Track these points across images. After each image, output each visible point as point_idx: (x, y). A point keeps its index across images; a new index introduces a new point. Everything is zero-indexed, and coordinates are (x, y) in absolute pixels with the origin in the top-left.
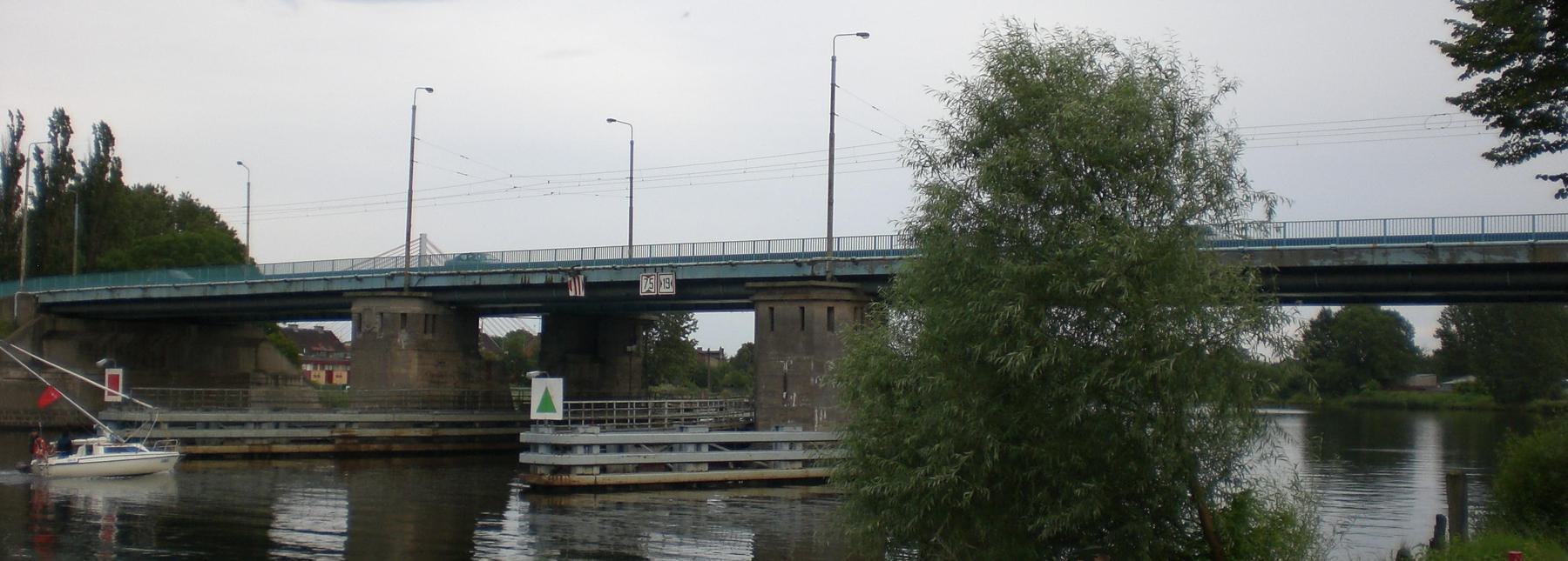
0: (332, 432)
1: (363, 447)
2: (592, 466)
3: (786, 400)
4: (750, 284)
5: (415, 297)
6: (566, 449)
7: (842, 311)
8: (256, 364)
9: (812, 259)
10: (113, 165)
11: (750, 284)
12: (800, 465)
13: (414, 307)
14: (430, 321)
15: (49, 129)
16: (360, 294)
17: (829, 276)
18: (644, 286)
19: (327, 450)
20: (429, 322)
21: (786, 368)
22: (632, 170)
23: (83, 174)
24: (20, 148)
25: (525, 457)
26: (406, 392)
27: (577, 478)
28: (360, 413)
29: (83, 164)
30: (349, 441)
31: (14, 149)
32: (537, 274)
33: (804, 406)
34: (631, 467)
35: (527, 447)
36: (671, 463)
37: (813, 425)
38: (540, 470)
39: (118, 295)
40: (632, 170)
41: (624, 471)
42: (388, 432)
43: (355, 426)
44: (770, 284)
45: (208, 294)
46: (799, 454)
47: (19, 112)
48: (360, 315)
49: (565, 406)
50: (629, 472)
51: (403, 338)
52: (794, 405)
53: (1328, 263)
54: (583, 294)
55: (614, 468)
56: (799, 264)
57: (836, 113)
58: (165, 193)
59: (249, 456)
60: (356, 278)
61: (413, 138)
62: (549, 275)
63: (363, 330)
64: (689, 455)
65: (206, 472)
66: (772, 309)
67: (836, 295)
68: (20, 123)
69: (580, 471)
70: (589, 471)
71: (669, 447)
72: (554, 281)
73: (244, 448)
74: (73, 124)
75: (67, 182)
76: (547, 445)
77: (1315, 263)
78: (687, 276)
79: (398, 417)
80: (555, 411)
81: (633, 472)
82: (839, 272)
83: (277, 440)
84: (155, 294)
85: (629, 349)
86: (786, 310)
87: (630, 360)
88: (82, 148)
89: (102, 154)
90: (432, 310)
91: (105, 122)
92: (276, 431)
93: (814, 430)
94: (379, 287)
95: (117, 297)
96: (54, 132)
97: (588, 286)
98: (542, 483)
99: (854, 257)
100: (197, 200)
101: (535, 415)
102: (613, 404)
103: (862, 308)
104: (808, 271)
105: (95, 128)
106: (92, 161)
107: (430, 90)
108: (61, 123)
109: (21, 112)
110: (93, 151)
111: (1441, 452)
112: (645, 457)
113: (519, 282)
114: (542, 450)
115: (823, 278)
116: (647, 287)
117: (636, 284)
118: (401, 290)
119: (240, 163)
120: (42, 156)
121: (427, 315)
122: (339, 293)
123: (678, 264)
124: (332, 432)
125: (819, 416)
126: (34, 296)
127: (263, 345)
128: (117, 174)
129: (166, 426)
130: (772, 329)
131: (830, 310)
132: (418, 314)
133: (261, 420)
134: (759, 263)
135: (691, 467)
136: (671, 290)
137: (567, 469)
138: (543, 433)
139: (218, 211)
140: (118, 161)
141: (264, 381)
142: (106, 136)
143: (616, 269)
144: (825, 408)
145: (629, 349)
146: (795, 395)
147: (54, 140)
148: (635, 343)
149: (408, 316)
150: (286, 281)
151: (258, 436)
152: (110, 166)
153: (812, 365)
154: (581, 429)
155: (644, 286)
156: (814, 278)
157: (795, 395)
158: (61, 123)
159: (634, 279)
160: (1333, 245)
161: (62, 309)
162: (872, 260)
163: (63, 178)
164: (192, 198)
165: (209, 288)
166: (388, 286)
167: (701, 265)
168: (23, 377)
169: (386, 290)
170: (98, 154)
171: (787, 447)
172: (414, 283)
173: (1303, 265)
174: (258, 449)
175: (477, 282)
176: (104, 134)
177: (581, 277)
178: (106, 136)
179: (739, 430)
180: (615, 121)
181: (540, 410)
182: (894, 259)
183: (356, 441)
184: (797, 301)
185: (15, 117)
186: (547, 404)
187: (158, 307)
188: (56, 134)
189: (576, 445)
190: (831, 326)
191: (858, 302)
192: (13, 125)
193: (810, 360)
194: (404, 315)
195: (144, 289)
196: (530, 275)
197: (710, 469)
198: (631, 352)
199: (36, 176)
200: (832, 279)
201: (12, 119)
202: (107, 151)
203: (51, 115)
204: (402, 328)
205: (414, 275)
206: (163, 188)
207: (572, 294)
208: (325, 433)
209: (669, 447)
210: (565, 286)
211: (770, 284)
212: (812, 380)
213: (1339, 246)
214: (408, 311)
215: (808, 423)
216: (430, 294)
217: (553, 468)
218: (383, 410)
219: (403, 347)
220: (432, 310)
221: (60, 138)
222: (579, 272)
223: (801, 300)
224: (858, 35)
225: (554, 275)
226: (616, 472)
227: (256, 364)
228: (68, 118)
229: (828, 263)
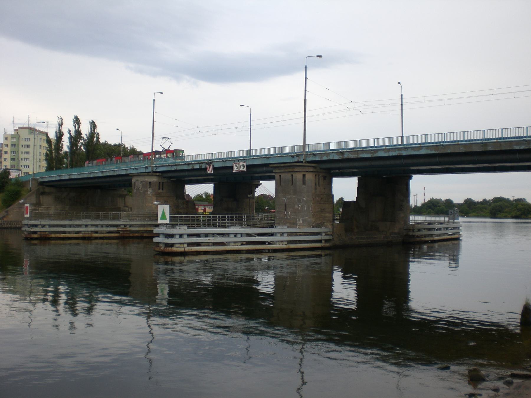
0: (118, 229)
1: (131, 235)
2: (183, 243)
3: (286, 215)
4: (271, 166)
5: (154, 175)
6: (172, 236)
7: (310, 177)
8: (125, 204)
9: (298, 155)
10: (96, 135)
11: (271, 166)
12: (286, 243)
13: (154, 179)
14: (161, 185)
15: (73, 123)
16: (134, 174)
17: (304, 161)
18: (234, 168)
19: (116, 236)
20: (161, 185)
21: (286, 201)
22: (250, 126)
23: (86, 138)
24: (62, 129)
25: (156, 240)
26: (151, 213)
27: (175, 249)
28: (130, 221)
29: (86, 135)
30: (125, 232)
31: (60, 130)
32: (196, 165)
33: (293, 217)
34: (245, 243)
35: (158, 235)
36: (226, 242)
37: (297, 226)
38: (161, 245)
39: (62, 178)
40: (250, 126)
41: (208, 245)
42: (142, 229)
43: (128, 226)
44: (279, 165)
45: (89, 177)
46: (286, 238)
47: (61, 117)
48: (135, 182)
49: (170, 217)
50: (210, 246)
51: (150, 192)
52: (289, 217)
53: (523, 147)
54: (212, 172)
55: (203, 244)
56: (293, 157)
57: (307, 90)
58: (125, 146)
59: (83, 238)
60: (135, 168)
61: (154, 112)
62: (201, 165)
63: (136, 189)
64: (231, 239)
65: (102, 244)
66: (280, 176)
67: (306, 169)
68: (62, 121)
69: (177, 245)
70: (182, 245)
71: (223, 235)
72: (202, 167)
73: (80, 235)
74: (81, 121)
75: (80, 141)
76: (163, 234)
77: (517, 148)
78: (251, 163)
79: (146, 223)
80: (166, 219)
81: (212, 246)
82: (308, 159)
83: (102, 232)
84: (73, 177)
85: (249, 196)
86: (286, 176)
87: (250, 200)
88: (85, 130)
89: (93, 131)
90: (161, 180)
91: (93, 120)
92: (85, 228)
93: (297, 228)
94: (143, 172)
95: (61, 179)
96: (75, 124)
97: (215, 169)
98: (161, 251)
99: (314, 154)
100: (136, 148)
101: (160, 221)
102: (237, 216)
103: (319, 175)
104: (296, 159)
105: (90, 122)
106: (90, 134)
107: (162, 93)
108: (77, 121)
109: (62, 117)
110: (90, 130)
111: (67, 240)
112: (209, 239)
113: (190, 168)
114: (161, 236)
115: (302, 162)
116: (235, 169)
117: (231, 167)
118: (150, 172)
119: (117, 129)
120: (71, 132)
121: (159, 183)
122: (127, 175)
123: (247, 158)
124: (118, 229)
125: (299, 221)
126: (37, 179)
127: (127, 197)
128: (98, 138)
129: (48, 227)
130: (281, 185)
131: (304, 176)
132: (156, 182)
133: (87, 224)
134: (277, 157)
135: (232, 244)
136: (244, 169)
137: (172, 245)
138: (162, 229)
139: (436, 196)
140: (98, 133)
141: (128, 210)
142: (93, 125)
143: (224, 161)
144: (302, 218)
145: (249, 196)
146: (289, 212)
147: (75, 127)
148: (252, 194)
149: (152, 182)
150: (112, 171)
151: (87, 230)
152: (95, 136)
153: (296, 200)
154: (178, 227)
155: (234, 168)
156: (298, 162)
157: (289, 212)
158: (77, 121)
159: (231, 165)
160: (524, 139)
161: (47, 184)
162: (322, 153)
163: (78, 140)
164: (134, 148)
165: (89, 174)
166: (146, 171)
167: (255, 158)
168: (32, 209)
169: (146, 172)
170: (91, 132)
171: (232, 236)
172: (155, 169)
173: (510, 149)
174: (86, 236)
175: (176, 169)
176: (93, 124)
177: (212, 165)
178: (93, 125)
179: (270, 228)
180: (243, 106)
181: (162, 219)
182: (330, 153)
183: (128, 232)
184: (290, 172)
185: (60, 119)
186: (163, 217)
187: (75, 182)
188: (75, 125)
189: (175, 234)
190: (304, 182)
191: (317, 172)
192: (59, 122)
193: (295, 198)
194: (150, 182)
195: (69, 175)
196: (194, 165)
197: (288, 244)
198: (250, 197)
199: (69, 140)
200: (305, 163)
201: (59, 119)
202: (94, 131)
203: (74, 118)
204: (150, 187)
205: (154, 166)
206: (124, 145)
207: (208, 172)
208: (115, 229)
209: (223, 235)
210: (206, 169)
211: (279, 165)
212: (296, 206)
213: (527, 139)
214: (151, 181)
215: (293, 224)
216: (160, 174)
217: (213, 243)
218: (144, 220)
219: (150, 195)
220: (161, 180)
221: (77, 126)
222: (211, 163)
223: (291, 172)
224: (317, 56)
225: (202, 165)
226: (204, 246)
227: (125, 204)
228: (79, 119)
229: (303, 155)
